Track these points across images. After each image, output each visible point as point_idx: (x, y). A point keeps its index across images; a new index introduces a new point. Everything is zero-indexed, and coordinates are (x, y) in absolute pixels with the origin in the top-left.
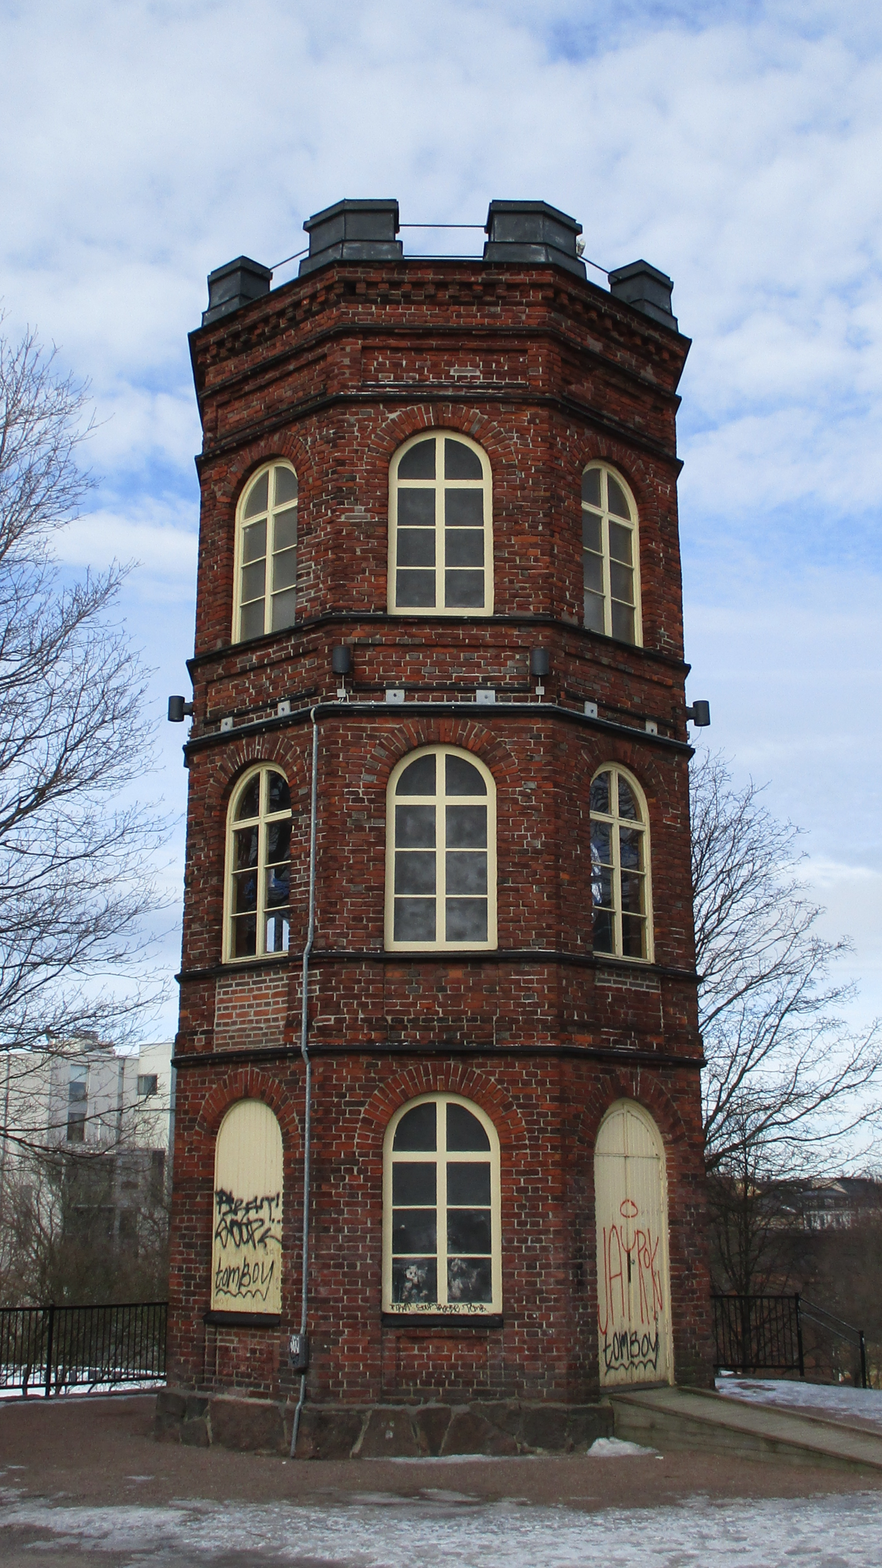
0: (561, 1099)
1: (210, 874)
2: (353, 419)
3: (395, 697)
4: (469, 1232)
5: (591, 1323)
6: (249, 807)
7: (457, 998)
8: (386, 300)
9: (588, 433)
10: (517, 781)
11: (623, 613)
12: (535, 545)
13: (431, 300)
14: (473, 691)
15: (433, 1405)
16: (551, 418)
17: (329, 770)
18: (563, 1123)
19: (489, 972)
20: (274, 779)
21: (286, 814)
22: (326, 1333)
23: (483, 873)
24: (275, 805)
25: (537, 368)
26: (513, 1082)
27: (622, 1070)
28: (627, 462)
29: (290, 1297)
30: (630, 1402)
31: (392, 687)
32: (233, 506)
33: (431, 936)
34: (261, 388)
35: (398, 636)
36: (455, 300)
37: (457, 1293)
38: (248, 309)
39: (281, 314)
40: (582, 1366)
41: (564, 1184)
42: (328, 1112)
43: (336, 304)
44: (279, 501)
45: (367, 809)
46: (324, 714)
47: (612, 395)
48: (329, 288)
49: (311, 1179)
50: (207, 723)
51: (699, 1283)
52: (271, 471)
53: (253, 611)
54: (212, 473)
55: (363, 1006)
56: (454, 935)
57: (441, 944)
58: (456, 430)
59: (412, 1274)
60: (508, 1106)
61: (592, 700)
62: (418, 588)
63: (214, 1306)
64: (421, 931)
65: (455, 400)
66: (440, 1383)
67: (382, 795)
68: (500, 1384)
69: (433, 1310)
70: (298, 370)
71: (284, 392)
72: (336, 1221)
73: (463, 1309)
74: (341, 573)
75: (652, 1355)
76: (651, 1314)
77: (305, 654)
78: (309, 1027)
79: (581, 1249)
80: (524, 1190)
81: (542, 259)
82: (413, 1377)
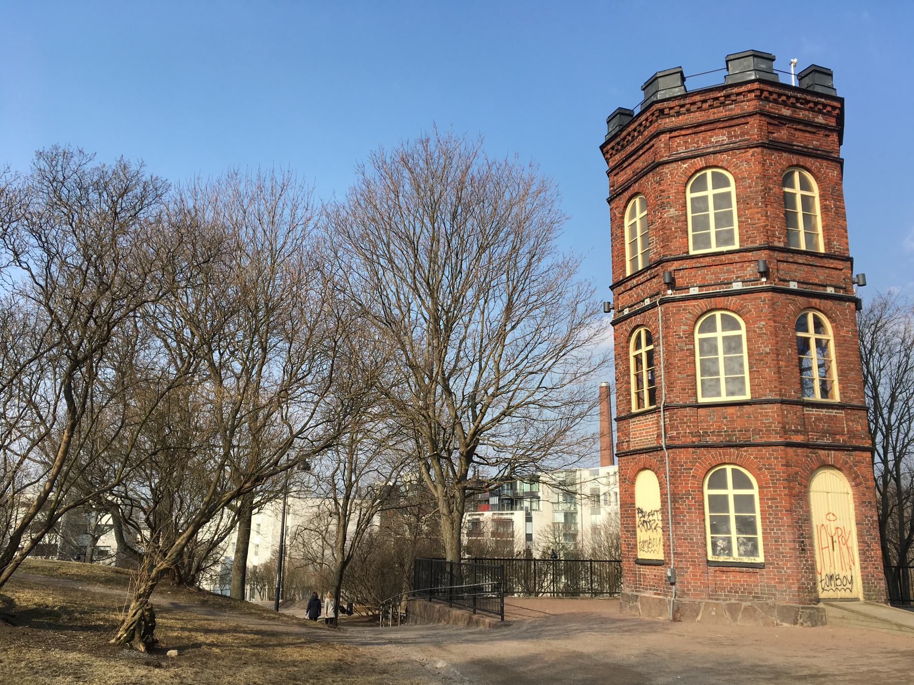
0: (787, 465)
1: (624, 375)
2: (667, 171)
3: (694, 291)
4: (746, 525)
5: (812, 568)
6: (638, 346)
7: (732, 421)
8: (678, 114)
9: (785, 155)
10: (755, 322)
11: (811, 237)
12: (758, 213)
13: (700, 109)
14: (731, 283)
15: (733, 601)
16: (762, 152)
17: (666, 327)
18: (789, 476)
19: (747, 408)
20: (647, 331)
21: (651, 347)
22: (682, 568)
23: (742, 365)
24: (648, 344)
25: (754, 129)
26: (762, 458)
27: (821, 452)
28: (808, 165)
29: (667, 553)
30: (832, 606)
31: (693, 287)
32: (623, 218)
33: (719, 394)
34: (630, 164)
35: (693, 263)
36: (711, 107)
37: (742, 552)
38: (621, 131)
39: (635, 130)
40: (807, 588)
41: (791, 504)
42: (676, 473)
43: (657, 121)
44: (642, 211)
45: (685, 341)
46: (662, 302)
47: (798, 134)
48: (653, 114)
49: (672, 502)
50: (619, 312)
51: (875, 554)
52: (637, 200)
53: (634, 260)
54: (613, 205)
55: (689, 427)
56: (730, 393)
57: (724, 398)
58: (716, 167)
59: (721, 544)
60: (760, 469)
61: (794, 281)
62: (702, 241)
63: (639, 557)
64: (714, 393)
65: (714, 153)
66: (736, 592)
67: (693, 333)
68: (765, 594)
69: (731, 560)
70: (644, 153)
71: (639, 164)
72: (683, 520)
73: (746, 560)
74: (666, 241)
75: (849, 586)
76: (848, 567)
77: (654, 277)
78: (665, 437)
79: (802, 534)
80: (771, 507)
81: (753, 77)
82: (724, 589)
